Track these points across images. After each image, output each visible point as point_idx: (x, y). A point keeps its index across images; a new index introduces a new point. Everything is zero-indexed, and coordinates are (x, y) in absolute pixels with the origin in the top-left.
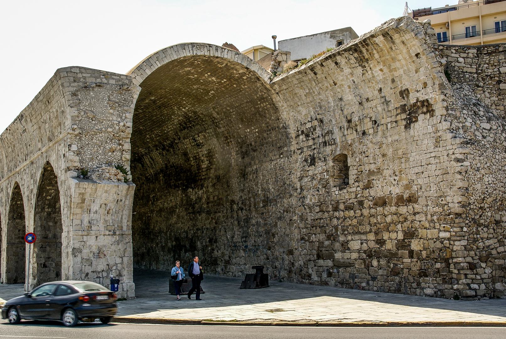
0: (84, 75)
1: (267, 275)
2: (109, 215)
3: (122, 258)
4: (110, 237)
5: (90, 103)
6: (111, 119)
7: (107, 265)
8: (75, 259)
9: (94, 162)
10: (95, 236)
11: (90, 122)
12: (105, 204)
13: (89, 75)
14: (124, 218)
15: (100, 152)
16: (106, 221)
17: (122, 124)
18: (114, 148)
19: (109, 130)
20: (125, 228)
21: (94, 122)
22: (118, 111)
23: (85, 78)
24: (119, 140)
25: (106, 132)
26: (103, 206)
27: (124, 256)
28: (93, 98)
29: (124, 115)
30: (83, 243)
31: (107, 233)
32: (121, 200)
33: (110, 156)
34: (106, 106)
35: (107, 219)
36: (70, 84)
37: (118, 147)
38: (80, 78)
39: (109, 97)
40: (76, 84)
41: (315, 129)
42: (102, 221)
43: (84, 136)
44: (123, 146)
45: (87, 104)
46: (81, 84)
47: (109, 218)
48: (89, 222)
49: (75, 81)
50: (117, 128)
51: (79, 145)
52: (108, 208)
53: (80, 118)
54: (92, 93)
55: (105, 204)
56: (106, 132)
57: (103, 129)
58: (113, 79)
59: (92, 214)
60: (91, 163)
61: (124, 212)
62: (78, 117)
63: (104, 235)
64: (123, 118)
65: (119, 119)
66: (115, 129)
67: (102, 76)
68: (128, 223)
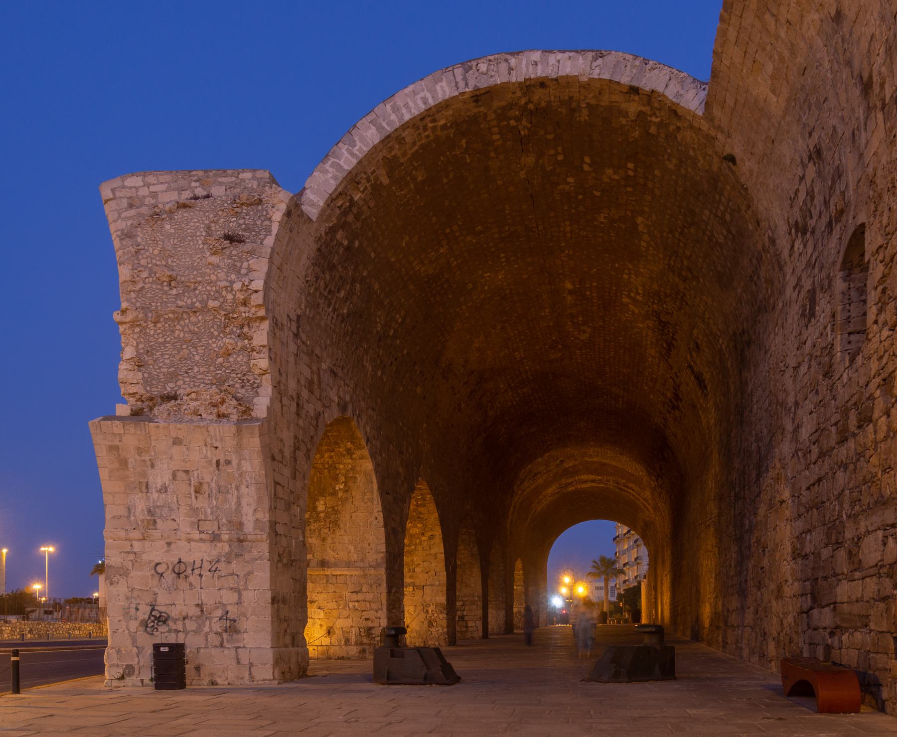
0: (153, 189)
1: (625, 590)
2: (200, 497)
3: (239, 592)
4: (204, 547)
5: (163, 250)
6: (213, 278)
7: (198, 605)
8: (111, 588)
9: (180, 383)
10: (163, 542)
11: (166, 293)
12: (187, 472)
13: (164, 187)
14: (244, 502)
15: (197, 358)
16: (195, 511)
17: (237, 286)
18: (230, 347)
19: (212, 304)
20: (249, 527)
21: (174, 292)
22: (230, 256)
23: (154, 195)
24: (242, 327)
25: (205, 309)
26: (180, 475)
27: (246, 589)
28: (169, 236)
29: (245, 264)
30: (132, 557)
31: (196, 535)
32: (228, 462)
33: (221, 366)
34: (202, 249)
35: (196, 504)
36: (119, 214)
37: (239, 344)
38: (144, 197)
39: (209, 228)
40: (133, 212)
41: (334, 551)
42: (184, 509)
43: (151, 325)
44: (250, 339)
45: (156, 252)
46: (144, 210)
47: (201, 503)
48: (149, 511)
49: (131, 206)
50: (230, 297)
51: (141, 346)
52: (194, 482)
53: (141, 285)
54: (168, 227)
55: (187, 472)
56: (205, 309)
57: (198, 305)
58: (221, 184)
59: (155, 495)
60: (171, 385)
61: (244, 490)
62: (134, 282)
63: (189, 541)
64: (243, 271)
65: (233, 277)
66: (226, 301)
67: (193, 184)
68: (260, 515)
